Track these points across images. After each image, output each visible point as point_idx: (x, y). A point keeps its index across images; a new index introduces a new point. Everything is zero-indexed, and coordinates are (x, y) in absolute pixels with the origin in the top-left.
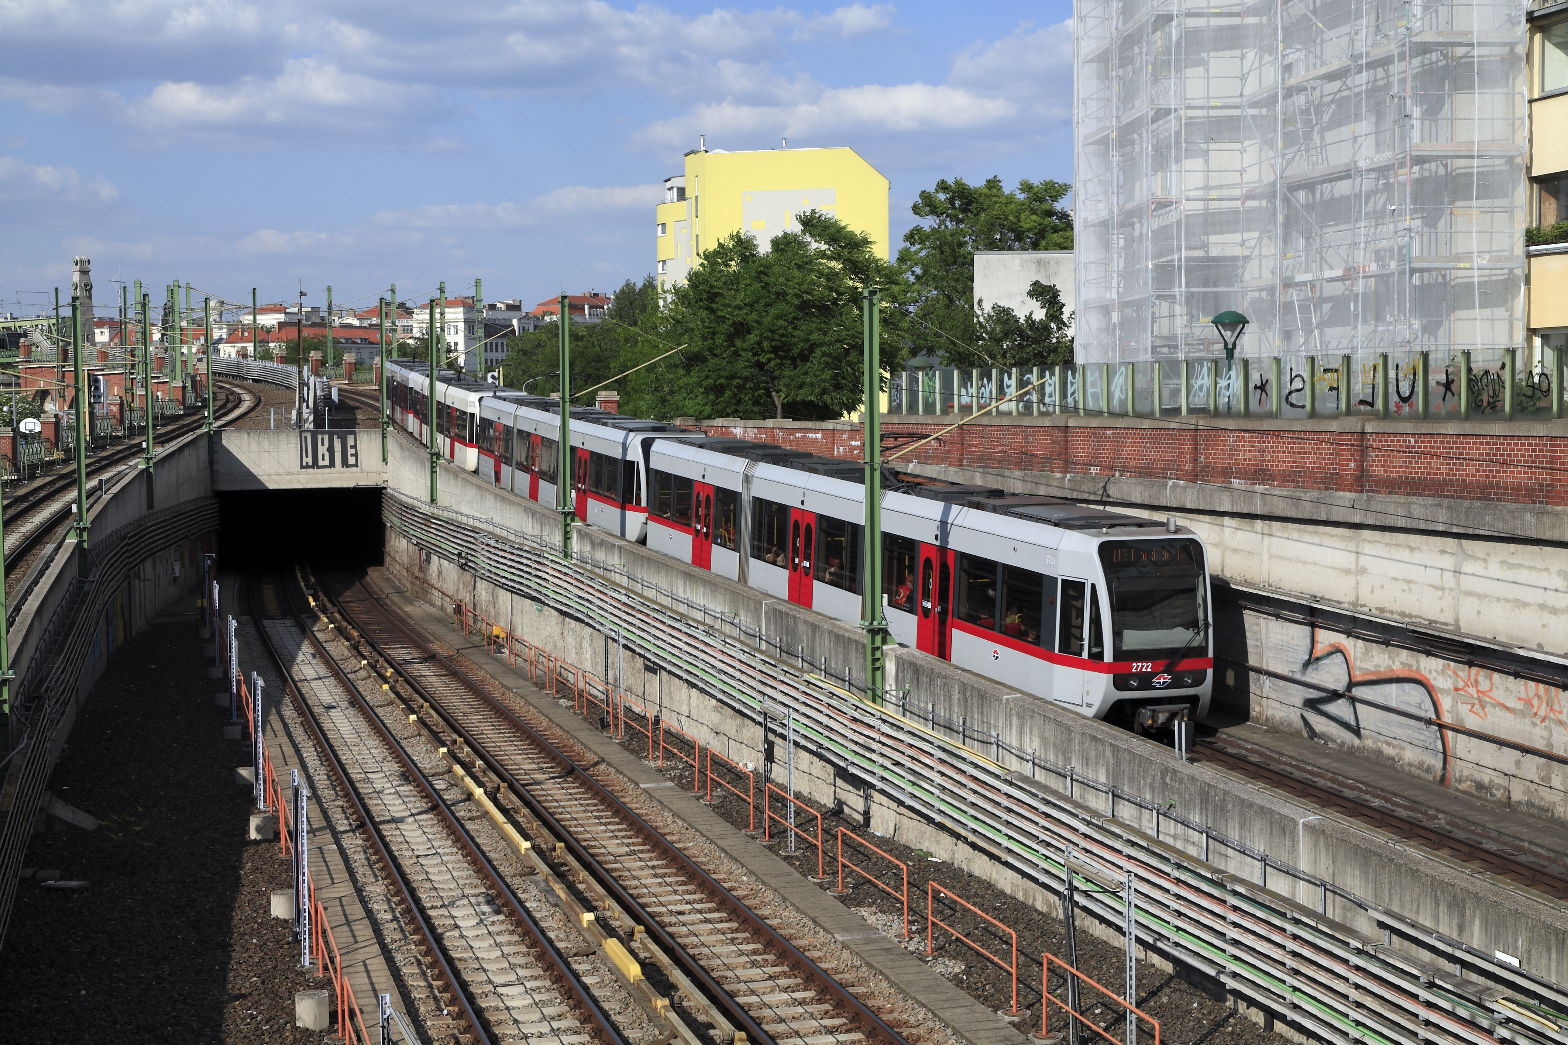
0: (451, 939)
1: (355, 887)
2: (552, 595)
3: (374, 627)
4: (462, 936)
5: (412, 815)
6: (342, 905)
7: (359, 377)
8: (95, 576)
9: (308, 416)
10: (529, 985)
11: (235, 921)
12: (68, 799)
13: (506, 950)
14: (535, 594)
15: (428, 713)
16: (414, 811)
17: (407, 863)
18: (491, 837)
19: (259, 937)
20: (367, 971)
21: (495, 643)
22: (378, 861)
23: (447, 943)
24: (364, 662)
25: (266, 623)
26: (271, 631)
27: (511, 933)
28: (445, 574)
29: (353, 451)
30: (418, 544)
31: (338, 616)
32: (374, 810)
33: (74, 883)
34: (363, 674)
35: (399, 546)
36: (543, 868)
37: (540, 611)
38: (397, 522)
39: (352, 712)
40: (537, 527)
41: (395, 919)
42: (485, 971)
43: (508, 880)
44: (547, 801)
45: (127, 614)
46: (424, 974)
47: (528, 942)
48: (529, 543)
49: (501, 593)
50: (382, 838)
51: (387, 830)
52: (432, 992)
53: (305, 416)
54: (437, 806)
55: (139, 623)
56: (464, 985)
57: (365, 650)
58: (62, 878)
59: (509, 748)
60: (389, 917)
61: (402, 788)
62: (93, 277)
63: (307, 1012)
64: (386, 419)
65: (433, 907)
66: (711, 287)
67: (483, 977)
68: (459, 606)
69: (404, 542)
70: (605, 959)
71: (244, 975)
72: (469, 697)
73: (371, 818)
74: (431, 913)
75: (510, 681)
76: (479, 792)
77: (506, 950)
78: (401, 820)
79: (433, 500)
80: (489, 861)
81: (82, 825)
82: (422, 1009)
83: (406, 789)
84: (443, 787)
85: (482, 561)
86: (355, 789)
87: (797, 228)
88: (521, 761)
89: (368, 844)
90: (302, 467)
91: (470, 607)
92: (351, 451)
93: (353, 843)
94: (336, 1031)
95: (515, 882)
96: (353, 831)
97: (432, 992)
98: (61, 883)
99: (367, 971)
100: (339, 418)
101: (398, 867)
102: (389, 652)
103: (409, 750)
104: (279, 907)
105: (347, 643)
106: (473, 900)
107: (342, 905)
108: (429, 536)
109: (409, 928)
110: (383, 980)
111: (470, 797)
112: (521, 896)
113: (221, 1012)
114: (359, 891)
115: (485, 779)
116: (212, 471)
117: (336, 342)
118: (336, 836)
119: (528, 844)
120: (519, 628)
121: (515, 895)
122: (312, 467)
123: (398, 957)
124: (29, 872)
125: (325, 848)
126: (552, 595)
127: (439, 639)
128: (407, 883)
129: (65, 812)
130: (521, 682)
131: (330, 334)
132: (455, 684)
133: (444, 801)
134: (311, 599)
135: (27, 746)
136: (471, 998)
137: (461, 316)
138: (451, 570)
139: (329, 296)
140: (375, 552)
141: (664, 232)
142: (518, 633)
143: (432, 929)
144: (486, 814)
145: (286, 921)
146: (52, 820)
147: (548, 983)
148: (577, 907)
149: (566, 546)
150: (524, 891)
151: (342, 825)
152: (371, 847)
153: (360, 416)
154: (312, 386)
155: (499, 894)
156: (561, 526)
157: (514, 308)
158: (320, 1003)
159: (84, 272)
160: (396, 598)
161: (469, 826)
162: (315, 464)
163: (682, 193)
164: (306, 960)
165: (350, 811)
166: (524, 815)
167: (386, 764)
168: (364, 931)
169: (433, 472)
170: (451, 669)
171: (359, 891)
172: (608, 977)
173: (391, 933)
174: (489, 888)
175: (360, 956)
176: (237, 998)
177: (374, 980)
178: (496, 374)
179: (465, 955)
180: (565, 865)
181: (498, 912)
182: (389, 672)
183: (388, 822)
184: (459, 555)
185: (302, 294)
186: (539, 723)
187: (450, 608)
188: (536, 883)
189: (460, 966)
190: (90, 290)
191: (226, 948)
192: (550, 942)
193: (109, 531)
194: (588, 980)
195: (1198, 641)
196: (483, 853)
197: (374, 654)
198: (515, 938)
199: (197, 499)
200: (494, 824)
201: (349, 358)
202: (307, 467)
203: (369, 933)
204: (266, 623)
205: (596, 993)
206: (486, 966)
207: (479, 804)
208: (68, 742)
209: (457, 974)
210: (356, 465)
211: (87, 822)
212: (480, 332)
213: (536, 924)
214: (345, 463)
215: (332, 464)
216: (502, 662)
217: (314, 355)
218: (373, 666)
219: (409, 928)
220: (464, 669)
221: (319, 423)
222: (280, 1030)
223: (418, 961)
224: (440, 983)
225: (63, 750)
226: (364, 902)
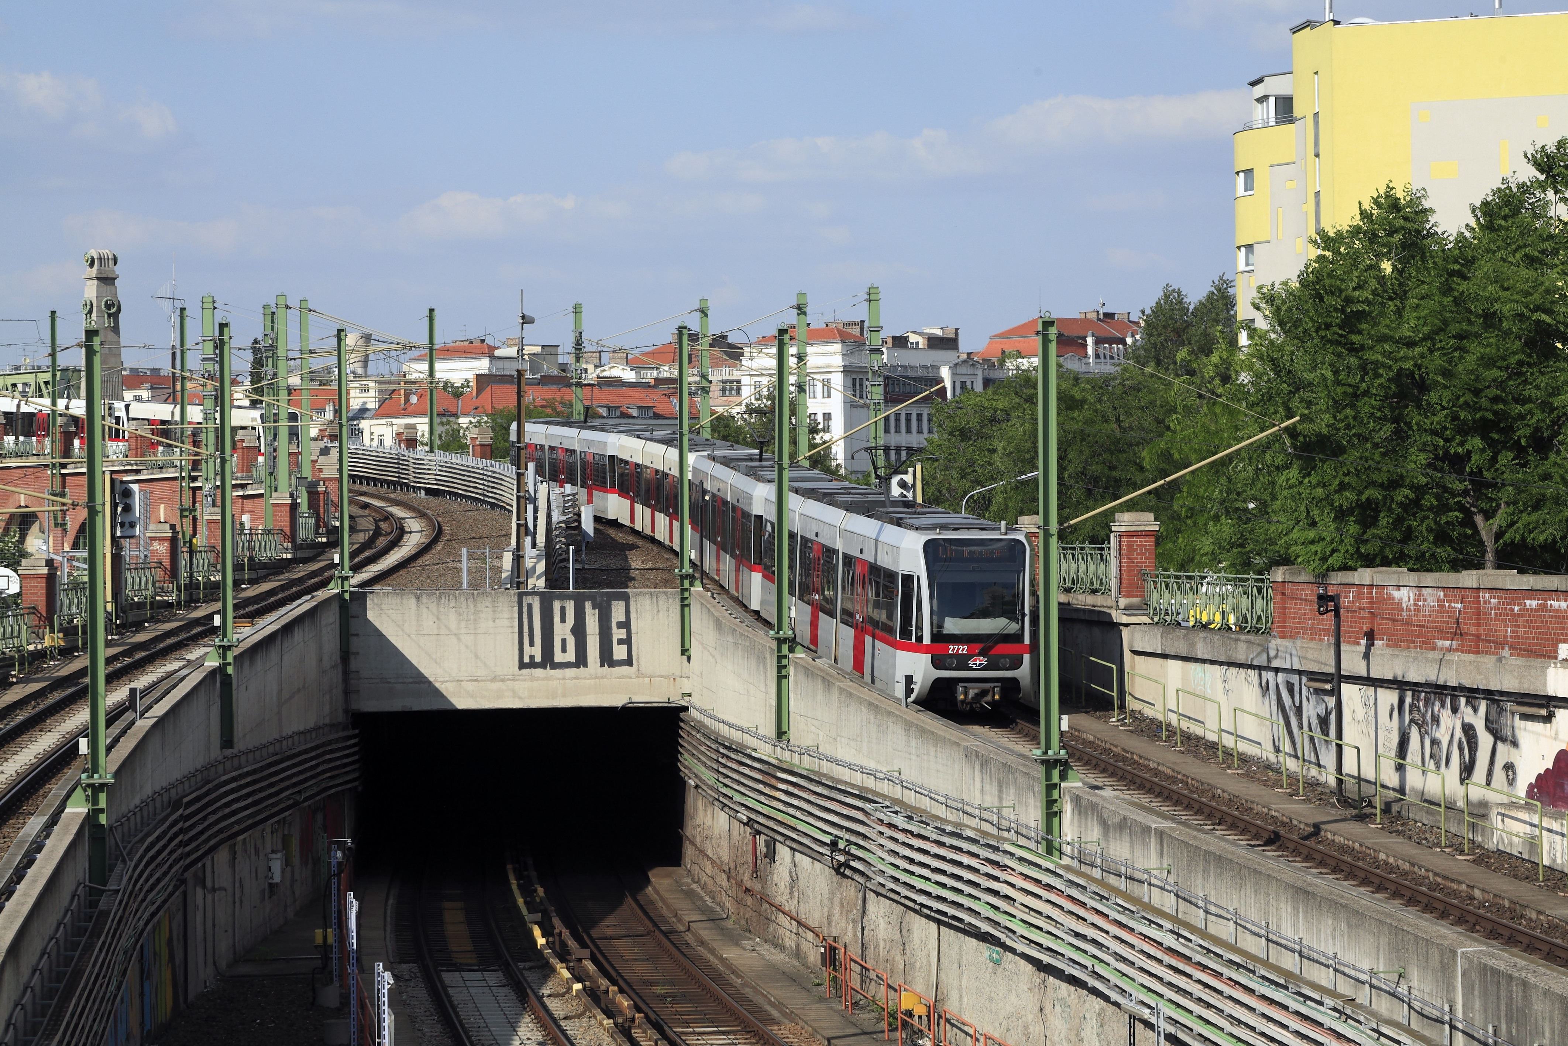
2: (1021, 929)
3: (659, 990)
8: (120, 879)
9: (535, 561)
14: (985, 927)
25: (448, 977)
26: (457, 995)
28: (804, 884)
29: (622, 634)
30: (749, 822)
31: (590, 966)
35: (712, 826)
37: (997, 963)
38: (708, 776)
40: (992, 789)
48: (975, 823)
49: (918, 923)
53: (528, 563)
55: (202, 977)
62: (123, 290)
66: (1348, 300)
68: (833, 950)
79: (781, 734)
85: (879, 858)
87: (1529, 173)
90: (522, 666)
92: (618, 634)
100: (595, 567)
105: (608, 1023)
108: (773, 807)
120: (954, 996)
122: (542, 665)
126: (1021, 929)
127: (792, 1017)
134: (537, 932)
138: (816, 876)
139: (577, 322)
140: (664, 838)
141: (1248, 186)
142: (952, 1007)
149: (1049, 829)
153: (636, 562)
157: (944, 343)
159: (106, 280)
160: (706, 932)
162: (548, 660)
163: (1285, 108)
169: (781, 677)
178: (908, 478)
184: (834, 845)
185: (526, 320)
187: (814, 954)
190: (115, 316)
193: (148, 791)
199: (317, 729)
202: (532, 665)
204: (448, 977)
210: (629, 662)
212: (877, 394)
214: (607, 659)
215: (581, 660)
221: (555, 577)
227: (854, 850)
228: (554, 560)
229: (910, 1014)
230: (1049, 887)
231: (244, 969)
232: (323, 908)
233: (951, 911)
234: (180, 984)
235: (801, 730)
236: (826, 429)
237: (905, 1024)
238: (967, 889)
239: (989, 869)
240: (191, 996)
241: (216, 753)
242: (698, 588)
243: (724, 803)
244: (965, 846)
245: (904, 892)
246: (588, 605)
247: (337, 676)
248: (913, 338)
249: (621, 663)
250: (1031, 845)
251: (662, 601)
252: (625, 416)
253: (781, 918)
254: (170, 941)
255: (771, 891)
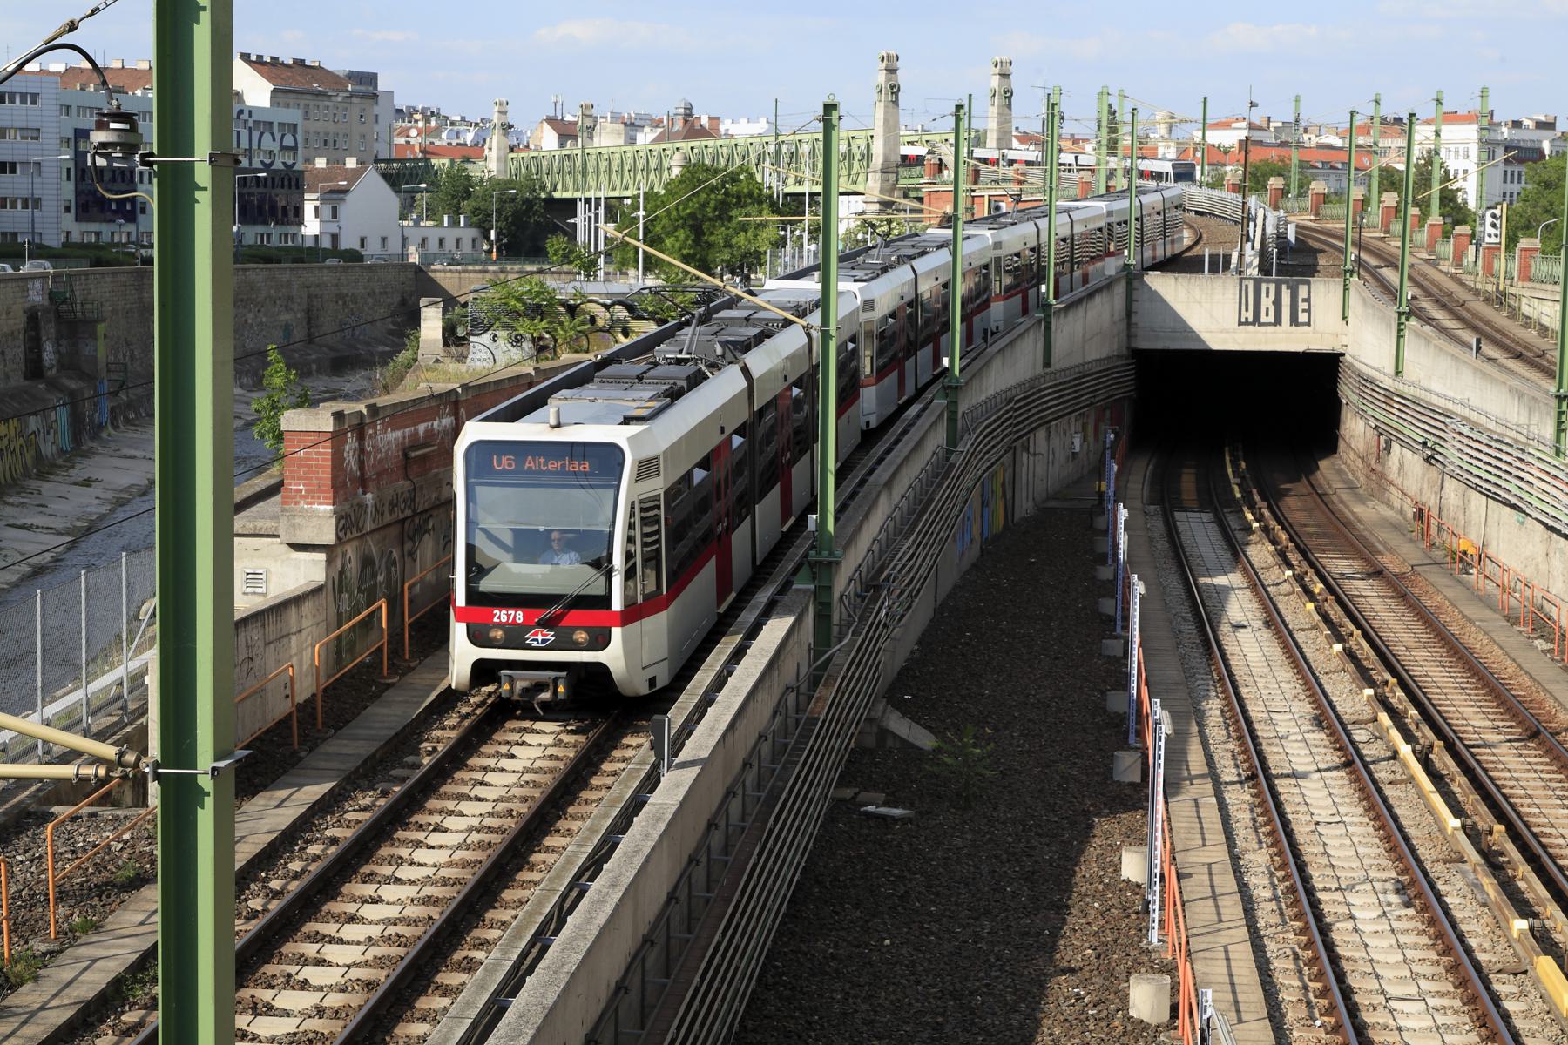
0: (1341, 934)
1: (1231, 852)
2: (1536, 503)
3: (1310, 530)
4: (1356, 930)
5: (1319, 770)
6: (1210, 874)
7: (1329, 212)
8: (965, 446)
9: (1252, 258)
10: (1432, 1002)
11: (1078, 879)
12: (906, 711)
13: (1410, 954)
14: (1514, 501)
15: (1358, 644)
16: (1322, 766)
17: (1301, 830)
18: (1414, 807)
19: (1103, 901)
20: (1228, 959)
21: (1462, 560)
22: (1266, 824)
23: (1335, 936)
24: (1289, 573)
25: (1178, 515)
26: (1181, 526)
27: (1421, 933)
28: (1406, 467)
29: (1305, 305)
30: (1376, 428)
31: (1266, 513)
32: (1272, 760)
33: (897, 812)
34: (1286, 587)
35: (1355, 429)
36: (1473, 855)
37: (1522, 523)
38: (1354, 398)
39: (1266, 633)
40: (1525, 413)
41: (1275, 898)
42: (1378, 977)
43: (1428, 865)
44: (1496, 769)
45: (1009, 495)
46: (1300, 971)
47: (1440, 947)
48: (1513, 434)
49: (1474, 495)
50: (1275, 795)
51: (1283, 786)
52: (1306, 995)
53: (1248, 259)
54: (1353, 762)
55: (1025, 506)
56: (1347, 993)
57: (1294, 558)
58: (886, 804)
59: (1458, 697)
60: (1268, 894)
61: (1311, 736)
62: (902, 78)
63: (1145, 999)
64: (1349, 266)
65: (1325, 889)
67: (1373, 984)
68: (1421, 510)
69: (1361, 423)
70: (1536, 984)
71: (1076, 947)
72: (1418, 627)
73: (1266, 769)
74: (1320, 895)
75: (1472, 611)
76: (1405, 750)
77: (1410, 954)
78: (1304, 776)
79: (1397, 373)
80: (1407, 839)
81: (918, 743)
82: (1290, 1015)
83: (1319, 737)
84: (1364, 738)
85: (1452, 453)
86: (1252, 732)
88: (1470, 714)
89: (1257, 801)
90: (1240, 323)
91: (1435, 512)
92: (1302, 306)
93: (1240, 799)
94: (1176, 1028)
95: (1435, 870)
96: (1241, 783)
97: (1306, 995)
98: (883, 810)
99: (1228, 959)
100: (1294, 261)
101: (1290, 834)
102: (1324, 562)
103: (1328, 689)
104: (1132, 866)
105: (1272, 548)
106: (1378, 886)
107: (1210, 874)
108: (1390, 419)
109: (1289, 912)
110: (1245, 972)
111: (1395, 756)
112: (1441, 886)
113: (1042, 986)
114: (1235, 858)
115: (1418, 734)
116: (1129, 324)
117: (1304, 166)
118: (1218, 786)
119: (1457, 823)
120: (1494, 543)
121: (1432, 885)
122: (1253, 324)
123: (1271, 947)
124: (848, 793)
125: (1201, 801)
126: (1536, 503)
127: (1391, 551)
128: (1297, 854)
129: (900, 726)
130: (1488, 614)
131: (1295, 156)
132: (1402, 609)
133: (1361, 757)
134: (1236, 489)
135: (853, 643)
136: (1353, 1010)
137: (1475, 136)
138: (1414, 461)
139: (1297, 107)
140: (1322, 432)
142: (1492, 551)
143: (1319, 916)
144: (1411, 779)
145: (1138, 885)
146: (884, 733)
147: (1457, 1003)
148: (1509, 910)
149: (1558, 441)
150: (1446, 882)
151: (1229, 773)
152: (1260, 805)
153: (1322, 261)
154: (1260, 221)
155: (1413, 882)
156: (1554, 413)
158: (1160, 989)
160: (1345, 495)
161: (1389, 791)
162: (1257, 320)
164: (1154, 936)
165: (1241, 758)
166: (1460, 785)
167: (1296, 703)
168: (1233, 908)
169: (1400, 337)
170: (1400, 590)
171: (1235, 858)
172: (1538, 1005)
173: (1266, 915)
174: (1402, 873)
175: (1223, 938)
176: (1063, 972)
177: (1234, 971)
178: (1498, 212)
179: (1356, 955)
180: (1502, 854)
181: (1408, 905)
182: (1318, 587)
183: (1288, 776)
184: (1425, 444)
185: (1253, 105)
186: (1502, 666)
187: (1410, 511)
188: (1464, 873)
189: (1346, 966)
190: (1009, 98)
191: (1062, 909)
192: (1469, 951)
193: (991, 392)
194: (1510, 1006)
195: (598, 589)
196: (1400, 828)
197: (1304, 563)
198: (1425, 940)
199: (1108, 358)
200: (1421, 795)
201: (1318, 187)
202: (1246, 323)
203: (1239, 911)
204: (1178, 515)
205: (1518, 1023)
206: (1380, 972)
207: (1405, 765)
208: (919, 643)
209: (1340, 977)
210: (1309, 324)
211: (924, 740)
212: (1501, 156)
213: (1454, 926)
214: (1294, 320)
215: (1278, 321)
216: (1467, 587)
217: (1275, 182)
218: (1299, 579)
219: (1289, 912)
220: (1417, 592)
221: (1265, 269)
222: (1109, 1018)
223: (1295, 954)
224: (1318, 985)
225: (912, 652)
226: (1238, 872)
227: (1437, 448)
228: (1264, 254)
229: (1465, 553)
230: (1555, 477)
231: (1052, 504)
232: (1099, 471)
233: (1494, 489)
234: (1009, 511)
235: (1411, 370)
236: (1464, 179)
237: (1461, 560)
238: (1505, 476)
239: (1518, 464)
240: (1016, 519)
241: (1039, 370)
242: (1355, 278)
243: (1361, 414)
244: (1505, 448)
245: (1466, 475)
246: (1284, 287)
247: (1123, 326)
248: (1526, 122)
249: (1303, 324)
250: (1546, 449)
251: (1332, 285)
252: (1333, 168)
253: (1392, 489)
254: (1003, 485)
255: (1387, 471)
